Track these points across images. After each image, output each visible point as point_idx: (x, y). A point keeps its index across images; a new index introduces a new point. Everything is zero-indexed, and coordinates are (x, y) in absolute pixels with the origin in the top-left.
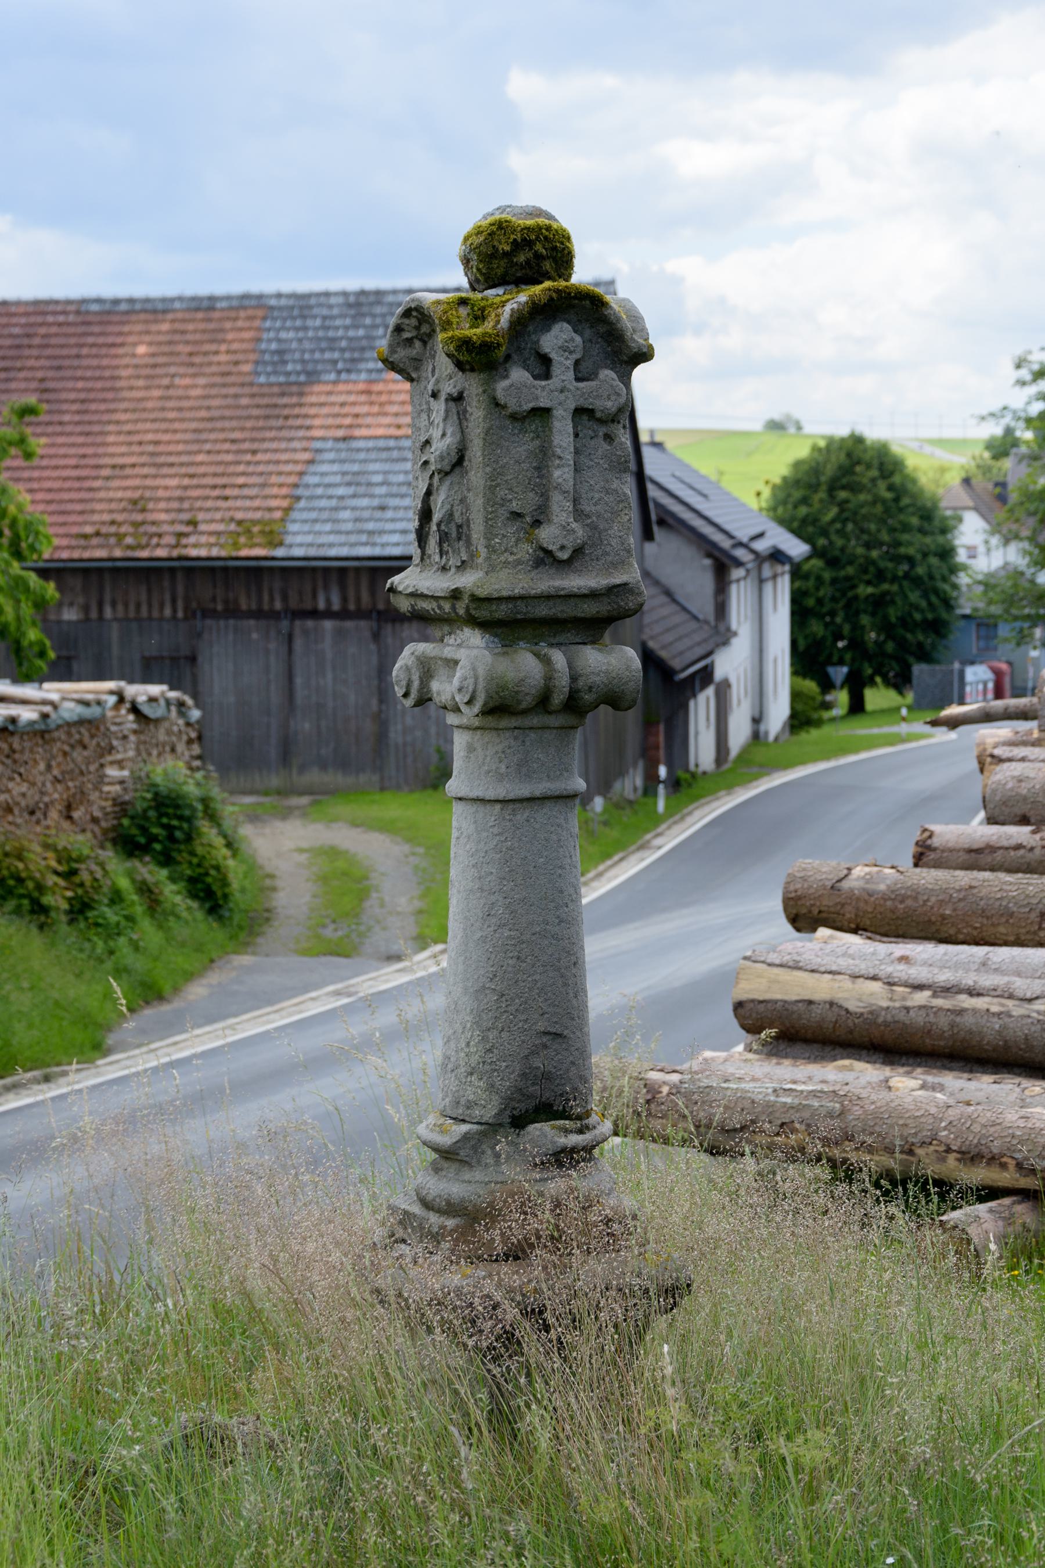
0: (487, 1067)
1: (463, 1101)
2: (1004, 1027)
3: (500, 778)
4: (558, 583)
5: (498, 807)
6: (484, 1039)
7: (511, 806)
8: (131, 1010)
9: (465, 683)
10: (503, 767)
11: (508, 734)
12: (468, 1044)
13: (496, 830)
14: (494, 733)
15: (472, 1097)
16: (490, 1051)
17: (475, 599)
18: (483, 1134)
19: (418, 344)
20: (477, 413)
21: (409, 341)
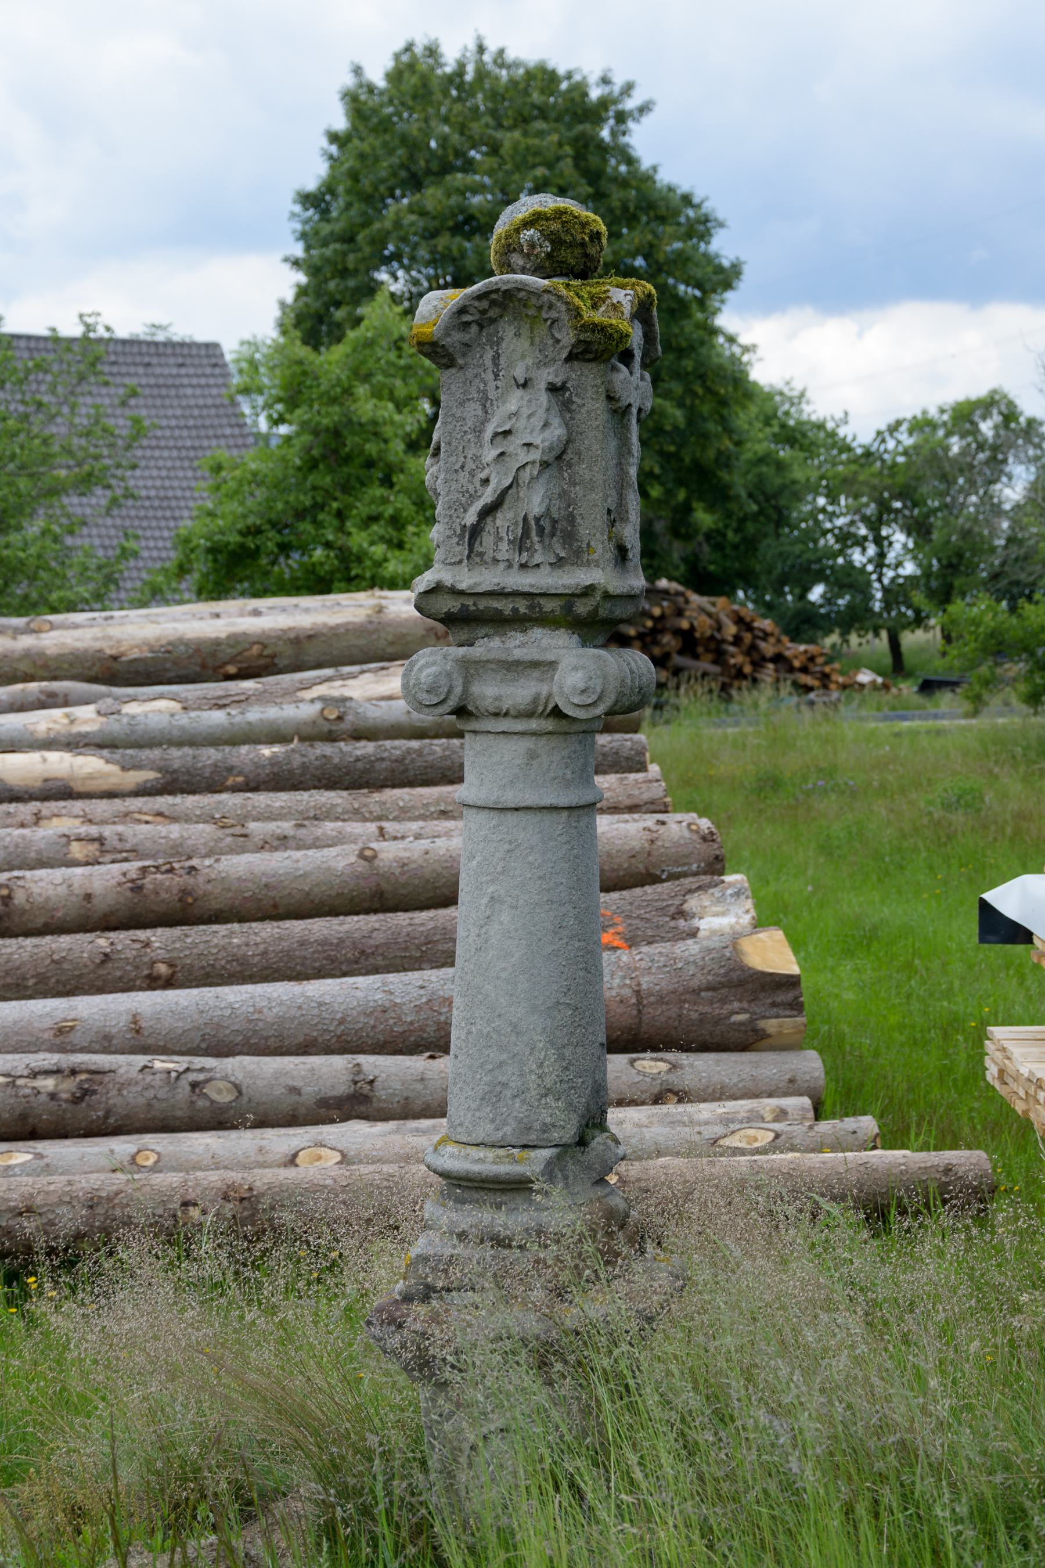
0: (565, 1086)
1: (537, 1125)
2: (185, 892)
3: (567, 784)
4: (26, 642)
5: (565, 814)
6: (561, 1057)
7: (576, 813)
8: (192, 1102)
9: (591, 683)
10: (568, 772)
11: (574, 738)
12: (541, 1065)
13: (564, 839)
14: (561, 738)
15: (548, 1120)
16: (566, 1068)
17: (607, 596)
18: (559, 1157)
19: (474, 328)
20: (593, 409)
21: (467, 324)
